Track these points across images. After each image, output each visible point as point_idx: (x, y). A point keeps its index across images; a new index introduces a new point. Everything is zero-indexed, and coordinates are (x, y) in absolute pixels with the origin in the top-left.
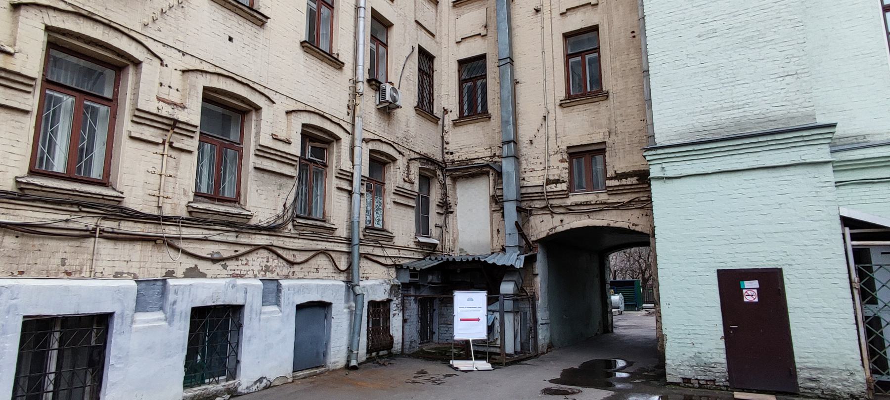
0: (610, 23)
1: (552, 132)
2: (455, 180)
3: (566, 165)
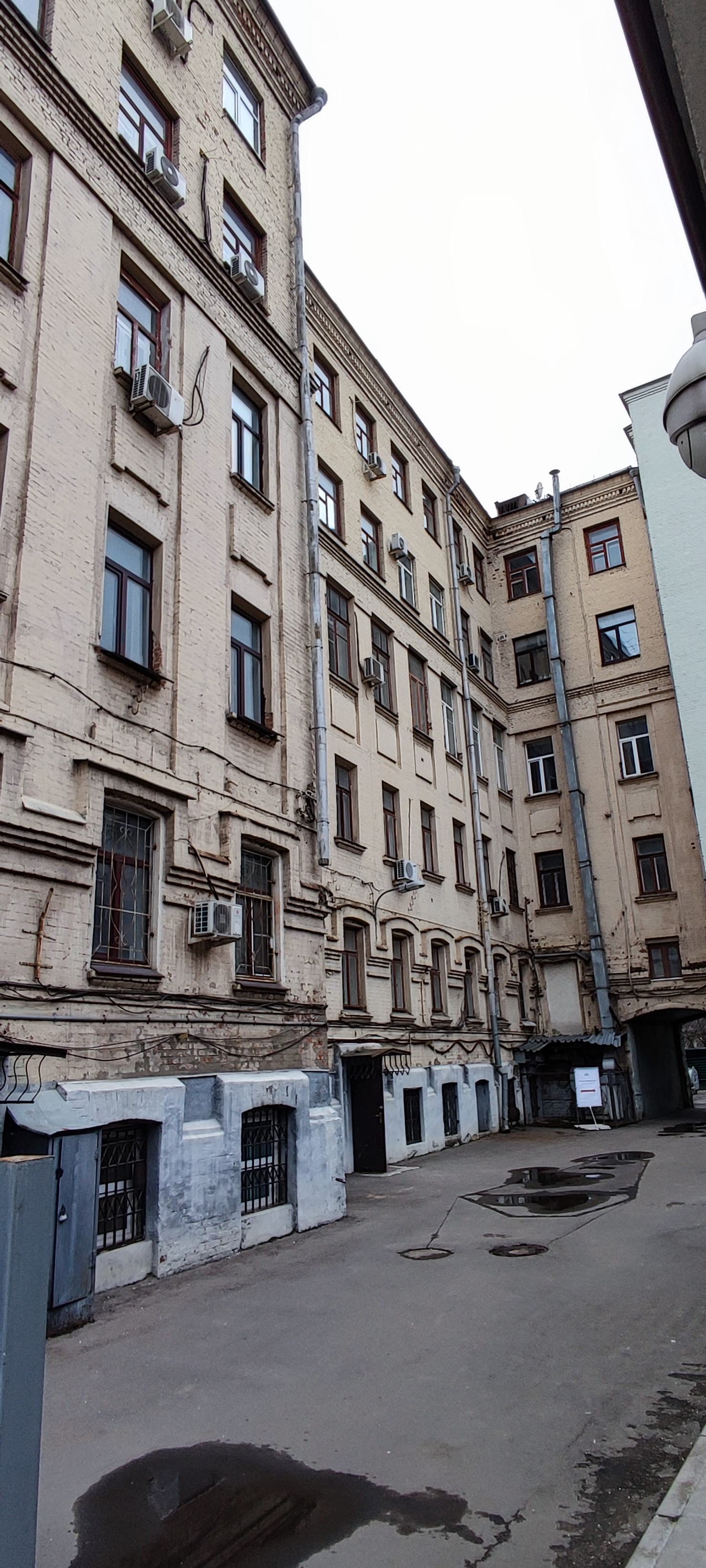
0: (673, 834)
1: (631, 926)
2: (542, 965)
3: (646, 955)
